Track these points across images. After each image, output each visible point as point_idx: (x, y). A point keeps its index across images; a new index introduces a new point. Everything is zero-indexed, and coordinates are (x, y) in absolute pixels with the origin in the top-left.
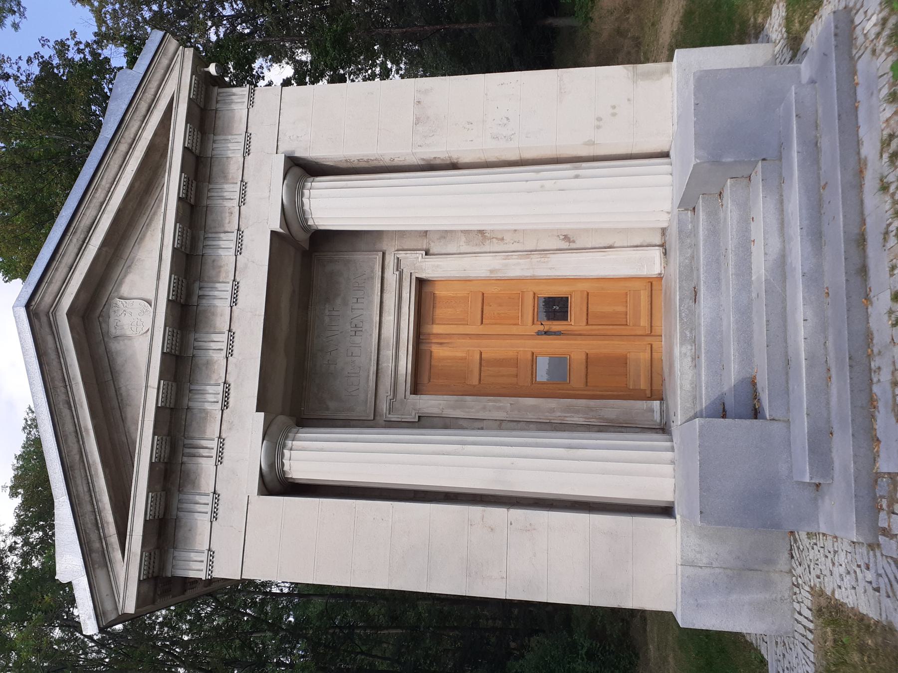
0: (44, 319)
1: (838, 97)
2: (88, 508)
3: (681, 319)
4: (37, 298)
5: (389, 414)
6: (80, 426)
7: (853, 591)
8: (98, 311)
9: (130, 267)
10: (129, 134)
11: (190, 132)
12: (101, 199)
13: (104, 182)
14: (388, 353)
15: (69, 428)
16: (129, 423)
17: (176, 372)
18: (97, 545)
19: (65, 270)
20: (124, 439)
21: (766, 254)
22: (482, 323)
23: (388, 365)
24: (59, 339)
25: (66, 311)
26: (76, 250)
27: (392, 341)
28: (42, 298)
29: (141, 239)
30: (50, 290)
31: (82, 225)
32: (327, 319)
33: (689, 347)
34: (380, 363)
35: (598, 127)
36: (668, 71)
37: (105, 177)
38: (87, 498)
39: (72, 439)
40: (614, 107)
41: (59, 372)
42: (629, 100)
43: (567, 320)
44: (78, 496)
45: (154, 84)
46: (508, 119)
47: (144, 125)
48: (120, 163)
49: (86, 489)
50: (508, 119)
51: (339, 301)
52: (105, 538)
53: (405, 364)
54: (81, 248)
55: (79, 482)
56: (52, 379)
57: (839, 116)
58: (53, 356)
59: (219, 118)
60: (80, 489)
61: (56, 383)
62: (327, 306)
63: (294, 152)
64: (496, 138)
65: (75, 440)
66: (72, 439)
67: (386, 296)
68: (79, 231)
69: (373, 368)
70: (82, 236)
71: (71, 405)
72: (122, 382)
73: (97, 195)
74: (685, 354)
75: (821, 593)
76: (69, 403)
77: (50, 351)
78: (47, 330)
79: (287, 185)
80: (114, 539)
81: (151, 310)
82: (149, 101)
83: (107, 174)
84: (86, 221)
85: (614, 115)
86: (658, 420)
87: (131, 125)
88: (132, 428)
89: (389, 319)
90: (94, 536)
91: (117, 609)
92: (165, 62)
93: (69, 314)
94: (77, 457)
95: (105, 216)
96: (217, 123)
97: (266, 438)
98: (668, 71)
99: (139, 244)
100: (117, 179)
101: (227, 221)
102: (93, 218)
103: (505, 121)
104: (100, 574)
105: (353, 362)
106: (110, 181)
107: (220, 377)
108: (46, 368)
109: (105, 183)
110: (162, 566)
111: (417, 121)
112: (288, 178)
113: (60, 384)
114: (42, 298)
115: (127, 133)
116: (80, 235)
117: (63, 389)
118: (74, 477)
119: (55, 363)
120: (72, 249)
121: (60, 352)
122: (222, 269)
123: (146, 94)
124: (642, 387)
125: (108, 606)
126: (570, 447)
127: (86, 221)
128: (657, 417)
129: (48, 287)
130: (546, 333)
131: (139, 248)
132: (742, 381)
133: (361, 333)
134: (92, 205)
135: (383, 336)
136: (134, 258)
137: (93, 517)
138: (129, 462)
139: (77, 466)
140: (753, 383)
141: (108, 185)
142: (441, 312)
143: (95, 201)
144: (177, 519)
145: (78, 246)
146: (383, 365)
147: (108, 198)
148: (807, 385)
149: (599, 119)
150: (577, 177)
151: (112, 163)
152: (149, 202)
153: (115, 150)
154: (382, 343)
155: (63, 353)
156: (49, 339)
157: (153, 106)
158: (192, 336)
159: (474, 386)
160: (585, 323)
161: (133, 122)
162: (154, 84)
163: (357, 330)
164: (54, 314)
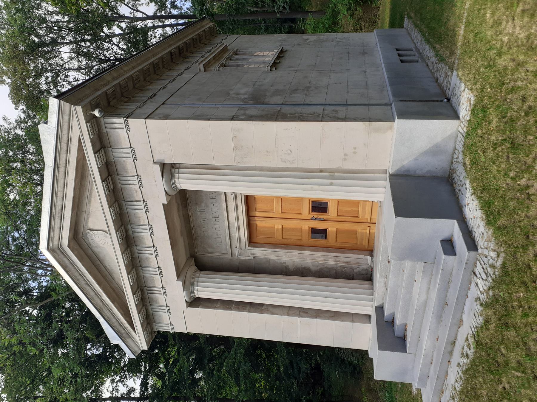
0: (58, 251)
1: (461, 283)
2: (114, 320)
3: (381, 268)
4: (51, 244)
5: (239, 255)
6: (97, 292)
7: (472, 202)
8: (81, 235)
9: (88, 214)
10: (62, 162)
11: (98, 158)
12: (62, 196)
13: (59, 188)
14: (234, 230)
15: (92, 294)
16: (116, 280)
17: (132, 263)
18: (123, 332)
19: (58, 230)
20: (117, 286)
21: (418, 300)
22: (282, 212)
23: (235, 235)
24: (69, 257)
25: (67, 246)
26: (59, 221)
27: (236, 225)
28: (53, 244)
29: (90, 201)
30: (55, 239)
31: (57, 210)
32: (199, 213)
33: (383, 279)
34: (231, 233)
35: (345, 159)
36: (391, 128)
37: (59, 186)
38: (112, 317)
39: (95, 298)
40: (355, 148)
41: (77, 272)
42: (365, 144)
43: (327, 212)
44: (108, 317)
45: (65, 132)
46: (291, 151)
47: (68, 154)
48: (64, 177)
49: (110, 314)
50: (291, 151)
51: (203, 205)
52: (125, 328)
53: (244, 234)
54: (61, 218)
55: (106, 312)
56: (75, 277)
57: (457, 298)
58: (70, 266)
59: (111, 136)
60: (108, 314)
61: (78, 277)
62: (197, 207)
63: (164, 160)
64: (283, 161)
65: (97, 297)
66: (95, 298)
67: (229, 204)
68: (57, 213)
69: (228, 237)
70: (60, 215)
71: (88, 284)
72: (106, 264)
73: (59, 195)
74: (381, 282)
75: (498, 9)
76: (87, 284)
77: (68, 265)
78: (62, 256)
79: (165, 181)
80: (129, 328)
81: (109, 235)
82: (66, 142)
83: (59, 184)
84: (58, 208)
85: (355, 153)
86: (370, 264)
87: (61, 157)
88: (119, 282)
89: (232, 215)
90: (121, 329)
91: (140, 349)
92: (66, 118)
93: (69, 246)
94: (101, 304)
95: (67, 202)
96: (110, 139)
97: (185, 290)
98: (391, 128)
99: (89, 203)
100: (66, 185)
101: (135, 195)
102: (62, 205)
103: (289, 152)
104: (129, 341)
105: (217, 232)
106: (62, 186)
107: (155, 264)
108: (70, 273)
109: (60, 189)
110: (152, 329)
111: (236, 148)
112: (164, 176)
113: (80, 277)
114: (53, 244)
115: (61, 162)
116: (58, 214)
117: (82, 279)
118: (103, 311)
119: (73, 269)
120: (57, 221)
121: (72, 264)
122: (141, 218)
123: (63, 139)
124: (366, 217)
125: (136, 349)
126: (326, 297)
127: (58, 208)
128: (369, 263)
129: (53, 239)
130: (315, 219)
131: (90, 206)
132: (401, 325)
133: (218, 220)
134: (58, 200)
135: (230, 222)
136: (89, 211)
137: (118, 323)
138: (123, 294)
139: (102, 307)
140: (406, 325)
141: (62, 189)
142: (259, 206)
143: (58, 198)
144: (153, 315)
145: (60, 219)
146: (232, 234)
147: (65, 194)
148: (422, 364)
149: (346, 155)
150: (331, 184)
151: (59, 178)
152: (86, 184)
153: (58, 172)
154: (230, 225)
155: (74, 263)
156: (65, 259)
157: (69, 143)
158: (135, 249)
159: (280, 240)
160: (336, 215)
161: (62, 156)
162: (65, 132)
163: (216, 219)
164: (62, 248)
